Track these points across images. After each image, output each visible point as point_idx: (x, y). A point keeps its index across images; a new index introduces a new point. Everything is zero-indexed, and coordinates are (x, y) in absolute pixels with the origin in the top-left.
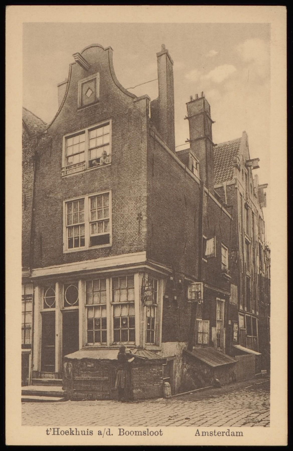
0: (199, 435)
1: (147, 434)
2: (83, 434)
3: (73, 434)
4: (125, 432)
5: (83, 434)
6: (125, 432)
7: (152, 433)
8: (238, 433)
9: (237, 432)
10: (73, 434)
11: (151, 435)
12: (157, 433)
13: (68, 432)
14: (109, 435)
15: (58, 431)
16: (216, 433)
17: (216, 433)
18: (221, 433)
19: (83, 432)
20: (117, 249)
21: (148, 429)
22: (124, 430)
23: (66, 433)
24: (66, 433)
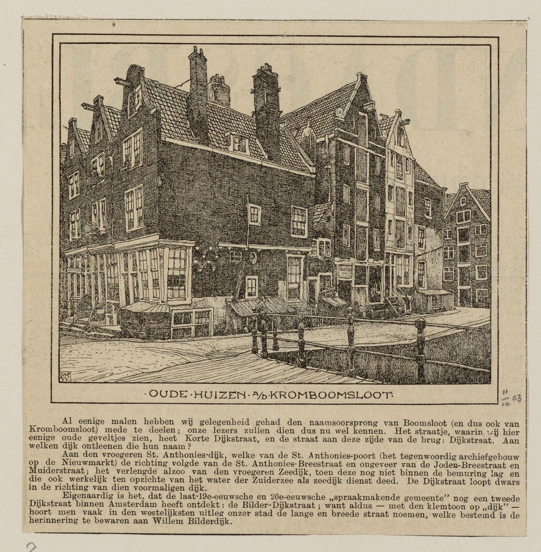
0: (167, 457)
1: (80, 430)
2: (309, 432)
3: (288, 507)
4: (409, 423)
5: (309, 432)
6: (409, 423)
7: (85, 430)
8: (152, 505)
9: (399, 439)
10: (288, 507)
11: (161, 395)
12: (89, 430)
13: (345, 431)
14: (394, 483)
15: (400, 431)
16: (221, 480)
17: (221, 480)
18: (225, 480)
19: (309, 431)
20: (255, 139)
21: (434, 504)
22: (409, 421)
23: (248, 472)
24: (248, 472)
